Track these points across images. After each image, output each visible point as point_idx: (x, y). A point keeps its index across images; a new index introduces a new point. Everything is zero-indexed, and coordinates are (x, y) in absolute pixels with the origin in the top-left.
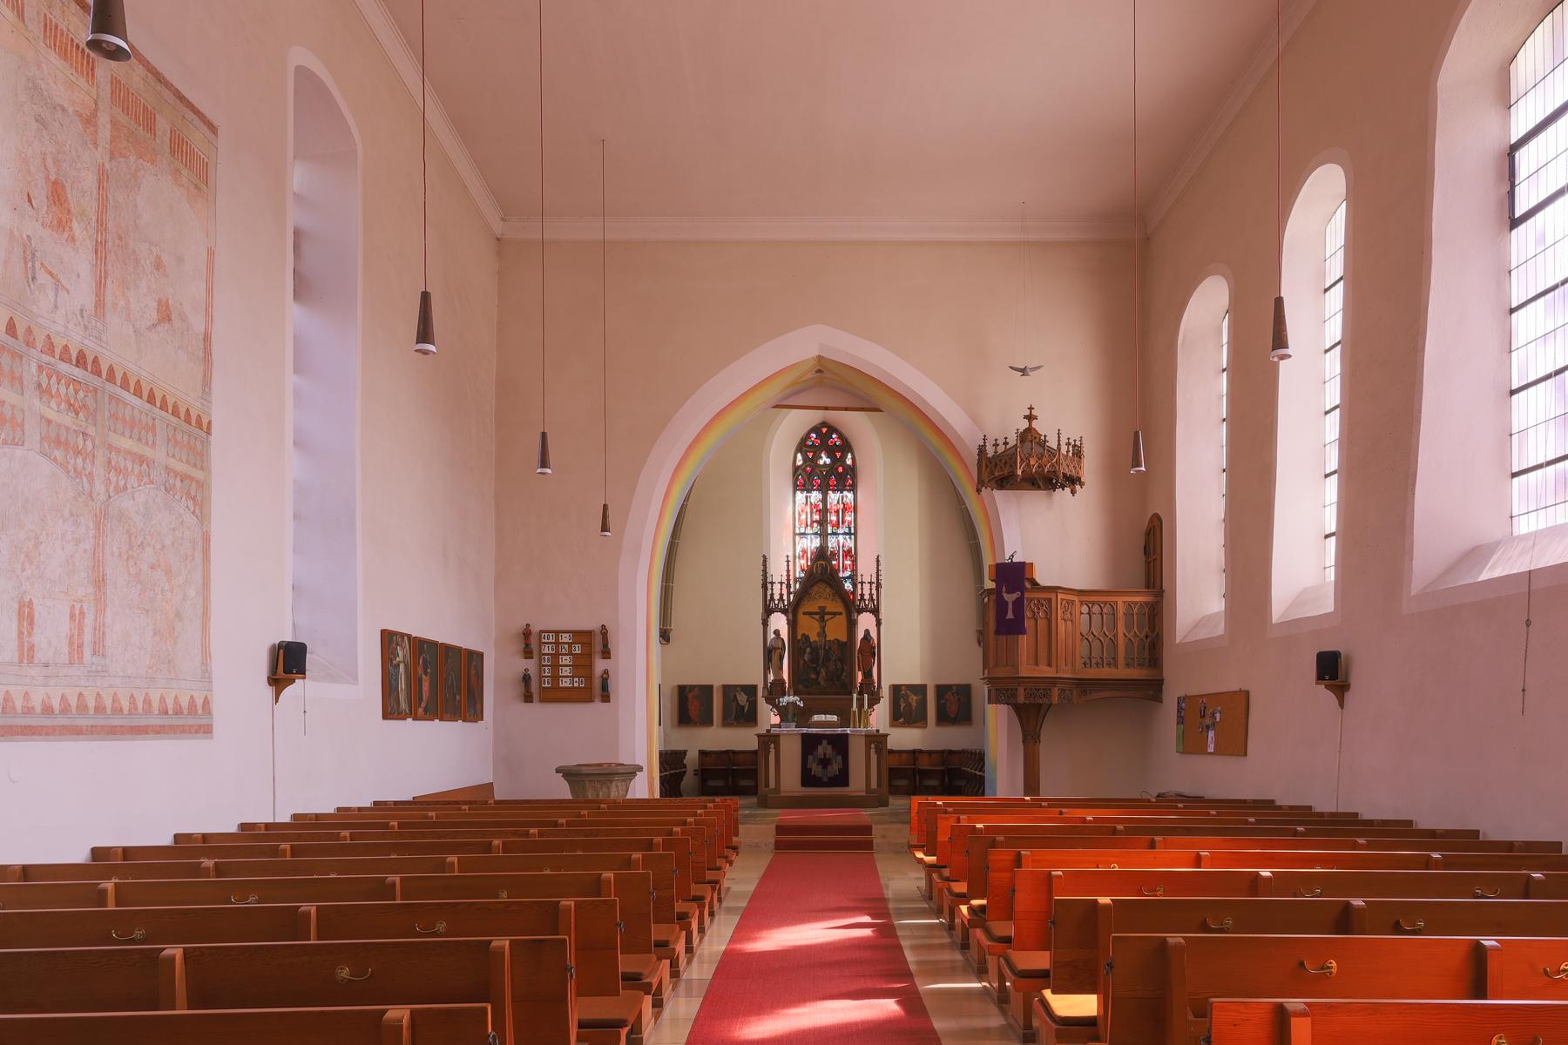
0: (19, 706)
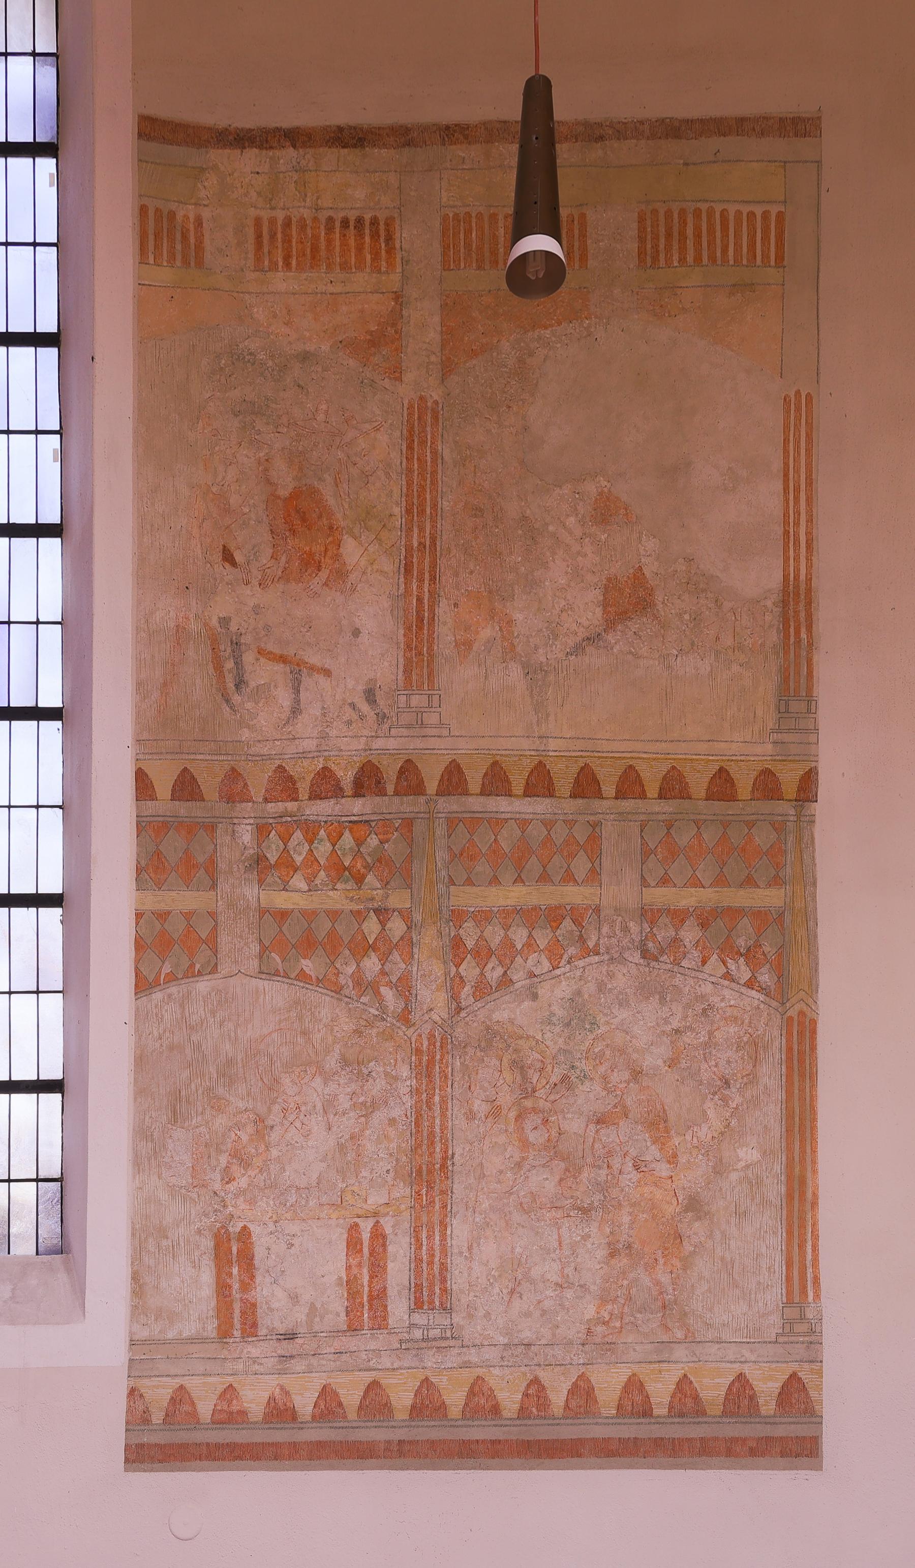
0: (205, 1409)
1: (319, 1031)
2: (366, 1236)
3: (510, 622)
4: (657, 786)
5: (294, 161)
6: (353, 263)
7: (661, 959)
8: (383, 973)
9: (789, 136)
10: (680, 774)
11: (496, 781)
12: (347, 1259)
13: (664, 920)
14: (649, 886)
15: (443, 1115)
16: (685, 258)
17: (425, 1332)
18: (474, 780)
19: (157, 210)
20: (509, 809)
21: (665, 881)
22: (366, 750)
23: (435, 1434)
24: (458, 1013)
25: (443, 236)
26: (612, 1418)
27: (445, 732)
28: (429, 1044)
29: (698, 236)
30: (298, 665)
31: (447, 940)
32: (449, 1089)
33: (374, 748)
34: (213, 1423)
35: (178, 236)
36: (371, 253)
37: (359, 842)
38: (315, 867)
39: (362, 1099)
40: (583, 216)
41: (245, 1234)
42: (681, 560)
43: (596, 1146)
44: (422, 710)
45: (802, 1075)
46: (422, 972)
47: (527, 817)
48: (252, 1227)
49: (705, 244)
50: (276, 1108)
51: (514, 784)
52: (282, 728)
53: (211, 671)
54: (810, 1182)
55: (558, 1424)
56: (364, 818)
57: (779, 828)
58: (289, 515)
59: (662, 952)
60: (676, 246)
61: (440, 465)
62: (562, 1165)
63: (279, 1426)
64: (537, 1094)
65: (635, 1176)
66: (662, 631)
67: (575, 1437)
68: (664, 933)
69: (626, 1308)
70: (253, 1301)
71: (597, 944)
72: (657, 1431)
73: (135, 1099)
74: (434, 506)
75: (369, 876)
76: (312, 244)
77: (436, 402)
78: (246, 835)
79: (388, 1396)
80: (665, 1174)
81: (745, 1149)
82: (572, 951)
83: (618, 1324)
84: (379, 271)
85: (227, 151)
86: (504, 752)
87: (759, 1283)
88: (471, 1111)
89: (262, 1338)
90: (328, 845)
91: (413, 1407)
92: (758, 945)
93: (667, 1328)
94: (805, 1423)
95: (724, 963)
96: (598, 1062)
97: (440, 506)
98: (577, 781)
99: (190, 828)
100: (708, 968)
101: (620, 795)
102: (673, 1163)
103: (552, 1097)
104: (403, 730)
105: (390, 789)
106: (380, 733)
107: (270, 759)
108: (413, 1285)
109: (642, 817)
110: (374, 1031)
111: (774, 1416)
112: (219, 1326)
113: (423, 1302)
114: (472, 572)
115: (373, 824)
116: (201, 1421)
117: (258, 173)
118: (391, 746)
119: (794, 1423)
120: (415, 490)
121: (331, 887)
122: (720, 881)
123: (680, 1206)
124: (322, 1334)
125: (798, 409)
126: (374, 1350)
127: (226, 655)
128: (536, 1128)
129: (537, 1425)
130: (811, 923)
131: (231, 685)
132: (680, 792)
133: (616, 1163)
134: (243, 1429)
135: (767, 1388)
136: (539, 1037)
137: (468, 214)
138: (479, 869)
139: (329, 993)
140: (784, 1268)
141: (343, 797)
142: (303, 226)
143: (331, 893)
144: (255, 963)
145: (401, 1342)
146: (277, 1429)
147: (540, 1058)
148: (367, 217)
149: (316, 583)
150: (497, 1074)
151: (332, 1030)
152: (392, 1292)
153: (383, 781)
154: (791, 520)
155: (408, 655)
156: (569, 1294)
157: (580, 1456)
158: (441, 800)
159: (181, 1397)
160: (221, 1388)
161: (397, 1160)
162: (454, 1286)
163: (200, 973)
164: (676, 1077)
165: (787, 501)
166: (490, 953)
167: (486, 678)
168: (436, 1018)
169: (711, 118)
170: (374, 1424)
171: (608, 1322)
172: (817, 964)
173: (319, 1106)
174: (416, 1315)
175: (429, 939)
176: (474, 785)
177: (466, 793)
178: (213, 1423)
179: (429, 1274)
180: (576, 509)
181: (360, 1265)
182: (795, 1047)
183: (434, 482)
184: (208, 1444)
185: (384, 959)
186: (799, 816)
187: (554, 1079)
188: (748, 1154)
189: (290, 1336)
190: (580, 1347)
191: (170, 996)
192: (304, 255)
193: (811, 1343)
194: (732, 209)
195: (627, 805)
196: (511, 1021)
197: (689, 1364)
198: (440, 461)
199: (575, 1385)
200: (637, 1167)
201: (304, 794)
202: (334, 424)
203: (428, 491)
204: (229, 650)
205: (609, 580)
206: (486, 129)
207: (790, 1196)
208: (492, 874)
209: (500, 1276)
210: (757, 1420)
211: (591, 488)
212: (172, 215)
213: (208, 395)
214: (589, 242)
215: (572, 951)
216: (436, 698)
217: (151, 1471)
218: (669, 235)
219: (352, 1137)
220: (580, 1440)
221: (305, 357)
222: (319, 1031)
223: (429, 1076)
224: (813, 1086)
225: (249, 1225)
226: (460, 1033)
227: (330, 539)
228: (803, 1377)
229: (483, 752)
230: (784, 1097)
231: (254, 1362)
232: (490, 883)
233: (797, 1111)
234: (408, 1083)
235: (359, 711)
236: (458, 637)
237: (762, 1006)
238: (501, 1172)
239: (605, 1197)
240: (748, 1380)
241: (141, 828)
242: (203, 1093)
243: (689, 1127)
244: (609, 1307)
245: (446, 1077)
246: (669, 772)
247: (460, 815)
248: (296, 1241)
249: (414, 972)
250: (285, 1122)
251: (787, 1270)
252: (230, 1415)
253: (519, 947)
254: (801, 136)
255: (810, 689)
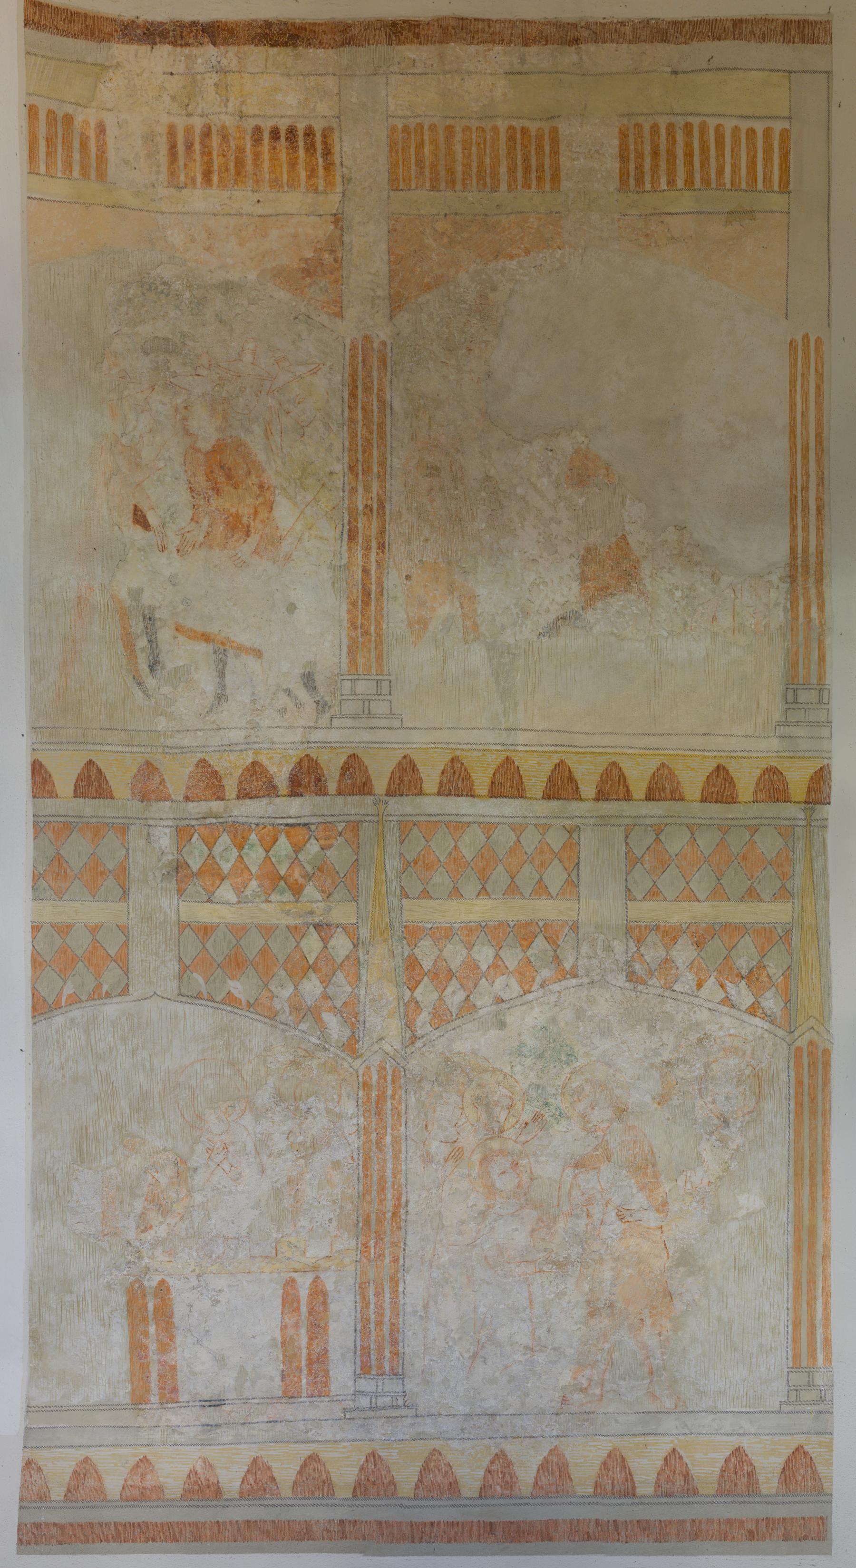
0: (113, 1485)
1: (250, 1062)
2: (304, 1293)
3: (473, 598)
4: (644, 785)
5: (213, 59)
6: (285, 181)
7: (650, 982)
8: (326, 997)
9: (794, 43)
10: (671, 773)
11: (456, 780)
12: (283, 1318)
13: (652, 938)
14: (635, 900)
15: (396, 1157)
16: (674, 181)
17: (374, 1400)
18: (431, 778)
19: (50, 112)
20: (471, 811)
21: (654, 893)
22: (303, 743)
23: (381, 1515)
24: (413, 1043)
25: (391, 151)
26: (588, 1497)
27: (396, 723)
28: (379, 1078)
29: (689, 155)
30: (223, 644)
31: (399, 959)
32: (403, 1129)
33: (312, 740)
34: (123, 1500)
35: (76, 144)
36: (306, 170)
37: (298, 848)
38: (246, 875)
39: (300, 1139)
40: (554, 131)
41: (163, 1289)
42: (671, 529)
43: (574, 1193)
44: (370, 697)
45: (813, 1112)
46: (371, 996)
47: (493, 820)
48: (170, 1281)
49: (697, 165)
50: (200, 1148)
51: (477, 783)
52: (205, 717)
53: (121, 649)
54: (820, 1232)
55: (526, 1504)
56: (302, 821)
57: (786, 832)
58: (212, 472)
59: (651, 974)
60: (663, 166)
61: (388, 416)
62: (534, 1214)
63: (200, 1503)
64: (505, 1134)
65: (618, 1226)
66: (650, 609)
67: (545, 1518)
68: (653, 953)
69: (607, 1374)
70: (173, 1363)
71: (575, 966)
72: (640, 1513)
73: (34, 1136)
74: (382, 464)
75: (308, 887)
76: (237, 157)
77: (384, 344)
78: (165, 839)
79: (328, 1472)
80: (653, 1224)
81: (746, 1195)
82: (546, 973)
83: (598, 1391)
84: (316, 191)
85: (134, 47)
86: (465, 747)
87: (761, 1345)
88: (428, 1154)
89: (184, 1404)
90: (261, 853)
91: (358, 1484)
92: (762, 966)
93: (654, 1396)
94: (812, 1502)
95: (722, 986)
96: (576, 1098)
97: (388, 463)
98: (551, 780)
99: (97, 830)
100: (704, 992)
101: (601, 796)
102: (663, 1211)
103: (523, 1138)
104: (347, 720)
105: (332, 787)
106: (320, 723)
107: (191, 752)
108: (359, 1348)
109: (627, 821)
110: (314, 1063)
111: (777, 1495)
112: (133, 1390)
113: (370, 1367)
114: (427, 540)
115: (313, 827)
116: (109, 1498)
117: (172, 74)
118: (334, 739)
119: (799, 1502)
120: (359, 444)
121: (263, 898)
122: (717, 894)
123: (670, 1260)
124: (253, 1401)
125: (806, 356)
126: (313, 1420)
127: (141, 636)
128: (503, 1173)
129: (501, 1505)
130: (823, 942)
131: (144, 667)
132: (671, 792)
133: (597, 1212)
134: (157, 1507)
135: (768, 1464)
136: (507, 1070)
137: (420, 126)
138: (437, 879)
139: (262, 1018)
140: (790, 1328)
141: (277, 796)
142: (225, 137)
143: (264, 906)
144: (174, 984)
145: (345, 1410)
146: (198, 1506)
147: (509, 1094)
148: (301, 126)
149: (246, 549)
150: (458, 1112)
151: (265, 1061)
152: (334, 1355)
153: (323, 779)
154: (799, 483)
155: (353, 634)
156: (541, 1358)
157: (550, 1539)
158: (392, 801)
159: (85, 1471)
160: (133, 1461)
161: (341, 1208)
162: (406, 1350)
163: (108, 995)
164: (667, 1115)
165: (794, 461)
166: (451, 975)
167: (444, 661)
168: (387, 1048)
169: (704, 20)
170: (311, 1502)
171: (586, 1389)
172: (830, 988)
173: (250, 1147)
174: (363, 1381)
175: (380, 959)
176: (431, 783)
177: (420, 793)
178: (123, 1500)
179: (377, 1336)
180: (548, 469)
181: (297, 1325)
182: (806, 1081)
183: (382, 435)
184: (116, 1524)
185: (326, 981)
186: (809, 820)
187: (526, 1117)
188: (751, 1200)
189: (216, 1403)
190: (554, 1417)
191: (72, 1020)
192: (227, 170)
193: (820, 1412)
194: (728, 124)
195: (609, 808)
196: (474, 1052)
197: (680, 1437)
198: (388, 411)
199: (547, 1460)
200: (621, 1218)
201: (231, 791)
202: (263, 366)
203: (375, 445)
204: (141, 626)
205: (588, 550)
206: (440, 26)
207: (798, 1249)
208: (452, 885)
209: (460, 1338)
210: (757, 1499)
211: (566, 444)
212: (68, 120)
213: (115, 330)
214: (562, 159)
215: (546, 973)
216: (385, 685)
217: (49, 1553)
218: (655, 153)
219: (289, 1182)
220: (551, 1521)
221: (228, 287)
222: (250, 1062)
223: (379, 1113)
224: (826, 1125)
225: (168, 1279)
226: (414, 1064)
227: (261, 500)
228: (810, 1451)
229: (440, 746)
230: (792, 1137)
231: (174, 1431)
232: (450, 896)
233: (807, 1152)
234: (355, 1121)
235: (296, 698)
236: (411, 615)
237: (766, 1035)
238: (463, 1222)
239: (584, 1249)
240: (746, 1456)
241: (39, 827)
242: (114, 1130)
243: (682, 1172)
244: (588, 1372)
245: (399, 1115)
246: (658, 769)
247: (414, 819)
248: (222, 1298)
249: (362, 997)
250: (210, 1163)
251: (794, 1330)
252: (142, 1493)
253: (484, 968)
254: (809, 42)
255: (822, 675)
